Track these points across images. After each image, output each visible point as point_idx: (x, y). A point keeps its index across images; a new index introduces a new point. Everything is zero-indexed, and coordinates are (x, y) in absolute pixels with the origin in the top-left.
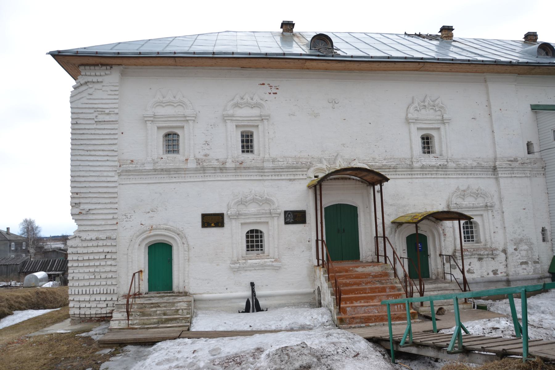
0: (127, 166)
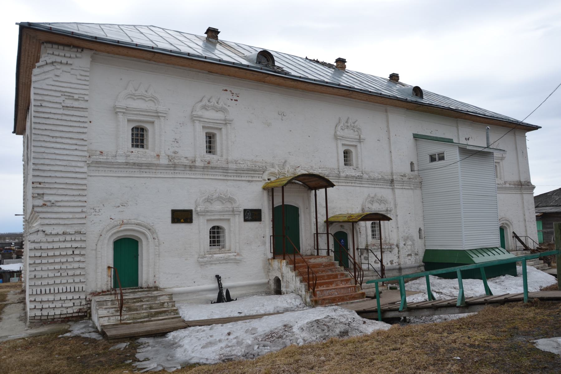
0: (98, 157)
